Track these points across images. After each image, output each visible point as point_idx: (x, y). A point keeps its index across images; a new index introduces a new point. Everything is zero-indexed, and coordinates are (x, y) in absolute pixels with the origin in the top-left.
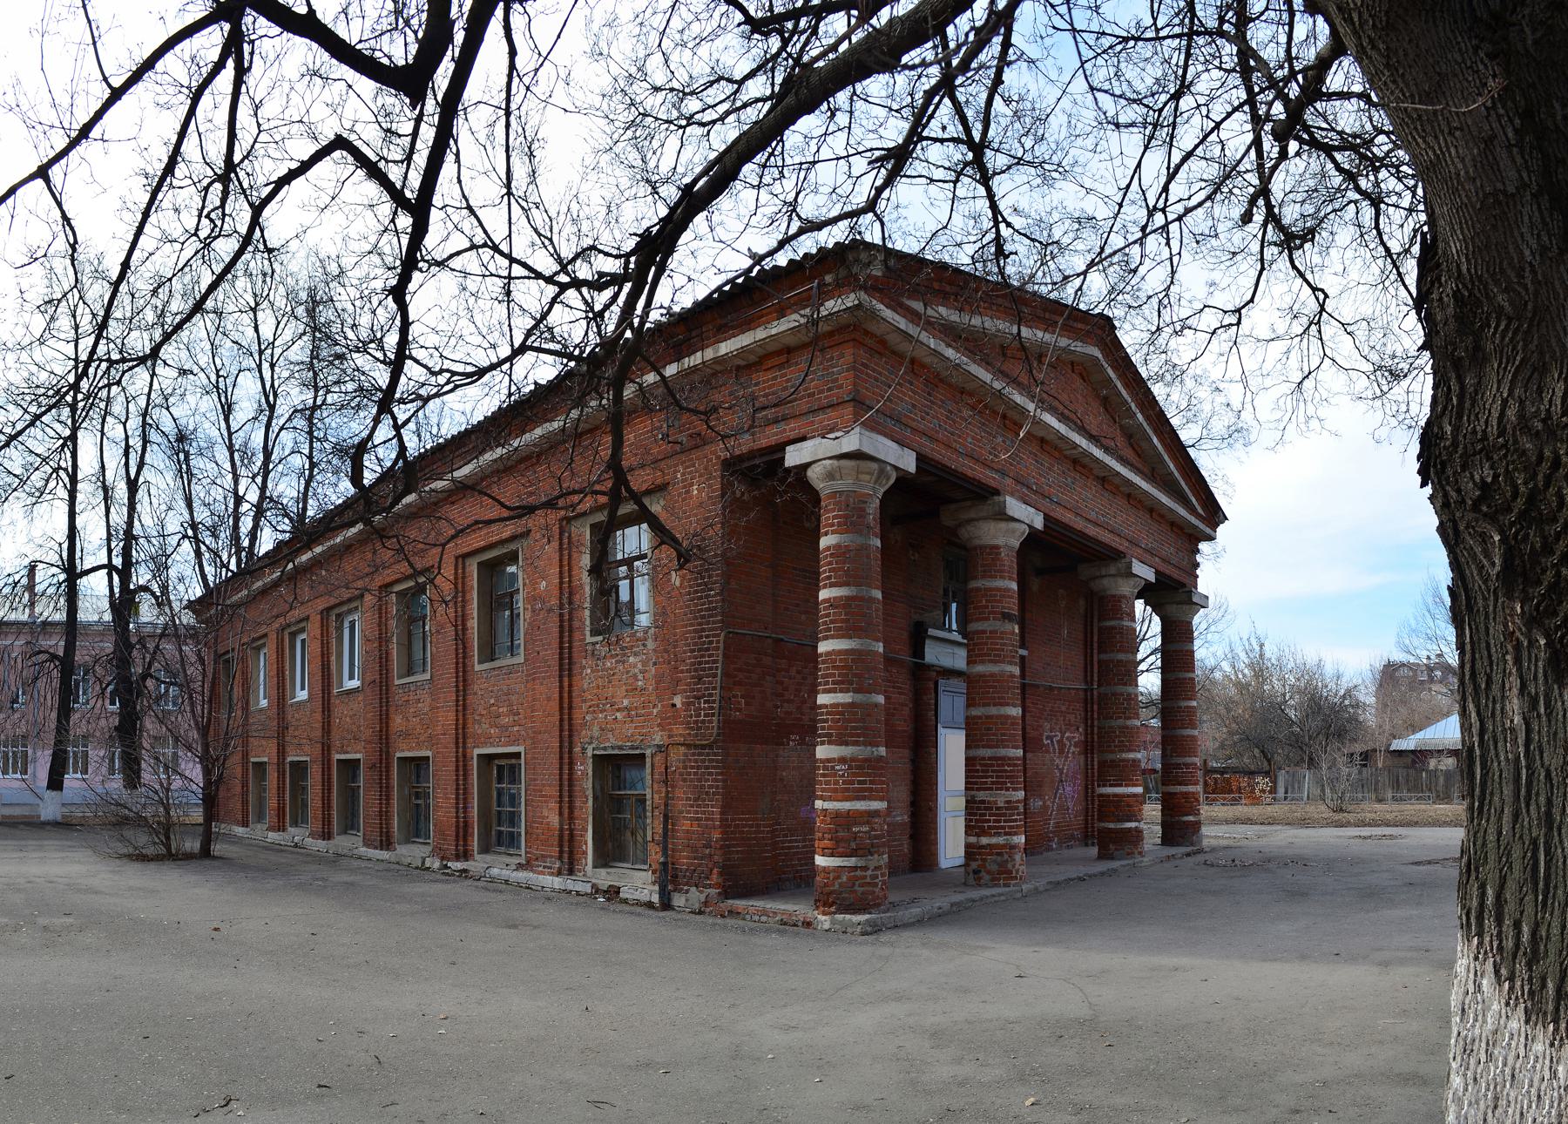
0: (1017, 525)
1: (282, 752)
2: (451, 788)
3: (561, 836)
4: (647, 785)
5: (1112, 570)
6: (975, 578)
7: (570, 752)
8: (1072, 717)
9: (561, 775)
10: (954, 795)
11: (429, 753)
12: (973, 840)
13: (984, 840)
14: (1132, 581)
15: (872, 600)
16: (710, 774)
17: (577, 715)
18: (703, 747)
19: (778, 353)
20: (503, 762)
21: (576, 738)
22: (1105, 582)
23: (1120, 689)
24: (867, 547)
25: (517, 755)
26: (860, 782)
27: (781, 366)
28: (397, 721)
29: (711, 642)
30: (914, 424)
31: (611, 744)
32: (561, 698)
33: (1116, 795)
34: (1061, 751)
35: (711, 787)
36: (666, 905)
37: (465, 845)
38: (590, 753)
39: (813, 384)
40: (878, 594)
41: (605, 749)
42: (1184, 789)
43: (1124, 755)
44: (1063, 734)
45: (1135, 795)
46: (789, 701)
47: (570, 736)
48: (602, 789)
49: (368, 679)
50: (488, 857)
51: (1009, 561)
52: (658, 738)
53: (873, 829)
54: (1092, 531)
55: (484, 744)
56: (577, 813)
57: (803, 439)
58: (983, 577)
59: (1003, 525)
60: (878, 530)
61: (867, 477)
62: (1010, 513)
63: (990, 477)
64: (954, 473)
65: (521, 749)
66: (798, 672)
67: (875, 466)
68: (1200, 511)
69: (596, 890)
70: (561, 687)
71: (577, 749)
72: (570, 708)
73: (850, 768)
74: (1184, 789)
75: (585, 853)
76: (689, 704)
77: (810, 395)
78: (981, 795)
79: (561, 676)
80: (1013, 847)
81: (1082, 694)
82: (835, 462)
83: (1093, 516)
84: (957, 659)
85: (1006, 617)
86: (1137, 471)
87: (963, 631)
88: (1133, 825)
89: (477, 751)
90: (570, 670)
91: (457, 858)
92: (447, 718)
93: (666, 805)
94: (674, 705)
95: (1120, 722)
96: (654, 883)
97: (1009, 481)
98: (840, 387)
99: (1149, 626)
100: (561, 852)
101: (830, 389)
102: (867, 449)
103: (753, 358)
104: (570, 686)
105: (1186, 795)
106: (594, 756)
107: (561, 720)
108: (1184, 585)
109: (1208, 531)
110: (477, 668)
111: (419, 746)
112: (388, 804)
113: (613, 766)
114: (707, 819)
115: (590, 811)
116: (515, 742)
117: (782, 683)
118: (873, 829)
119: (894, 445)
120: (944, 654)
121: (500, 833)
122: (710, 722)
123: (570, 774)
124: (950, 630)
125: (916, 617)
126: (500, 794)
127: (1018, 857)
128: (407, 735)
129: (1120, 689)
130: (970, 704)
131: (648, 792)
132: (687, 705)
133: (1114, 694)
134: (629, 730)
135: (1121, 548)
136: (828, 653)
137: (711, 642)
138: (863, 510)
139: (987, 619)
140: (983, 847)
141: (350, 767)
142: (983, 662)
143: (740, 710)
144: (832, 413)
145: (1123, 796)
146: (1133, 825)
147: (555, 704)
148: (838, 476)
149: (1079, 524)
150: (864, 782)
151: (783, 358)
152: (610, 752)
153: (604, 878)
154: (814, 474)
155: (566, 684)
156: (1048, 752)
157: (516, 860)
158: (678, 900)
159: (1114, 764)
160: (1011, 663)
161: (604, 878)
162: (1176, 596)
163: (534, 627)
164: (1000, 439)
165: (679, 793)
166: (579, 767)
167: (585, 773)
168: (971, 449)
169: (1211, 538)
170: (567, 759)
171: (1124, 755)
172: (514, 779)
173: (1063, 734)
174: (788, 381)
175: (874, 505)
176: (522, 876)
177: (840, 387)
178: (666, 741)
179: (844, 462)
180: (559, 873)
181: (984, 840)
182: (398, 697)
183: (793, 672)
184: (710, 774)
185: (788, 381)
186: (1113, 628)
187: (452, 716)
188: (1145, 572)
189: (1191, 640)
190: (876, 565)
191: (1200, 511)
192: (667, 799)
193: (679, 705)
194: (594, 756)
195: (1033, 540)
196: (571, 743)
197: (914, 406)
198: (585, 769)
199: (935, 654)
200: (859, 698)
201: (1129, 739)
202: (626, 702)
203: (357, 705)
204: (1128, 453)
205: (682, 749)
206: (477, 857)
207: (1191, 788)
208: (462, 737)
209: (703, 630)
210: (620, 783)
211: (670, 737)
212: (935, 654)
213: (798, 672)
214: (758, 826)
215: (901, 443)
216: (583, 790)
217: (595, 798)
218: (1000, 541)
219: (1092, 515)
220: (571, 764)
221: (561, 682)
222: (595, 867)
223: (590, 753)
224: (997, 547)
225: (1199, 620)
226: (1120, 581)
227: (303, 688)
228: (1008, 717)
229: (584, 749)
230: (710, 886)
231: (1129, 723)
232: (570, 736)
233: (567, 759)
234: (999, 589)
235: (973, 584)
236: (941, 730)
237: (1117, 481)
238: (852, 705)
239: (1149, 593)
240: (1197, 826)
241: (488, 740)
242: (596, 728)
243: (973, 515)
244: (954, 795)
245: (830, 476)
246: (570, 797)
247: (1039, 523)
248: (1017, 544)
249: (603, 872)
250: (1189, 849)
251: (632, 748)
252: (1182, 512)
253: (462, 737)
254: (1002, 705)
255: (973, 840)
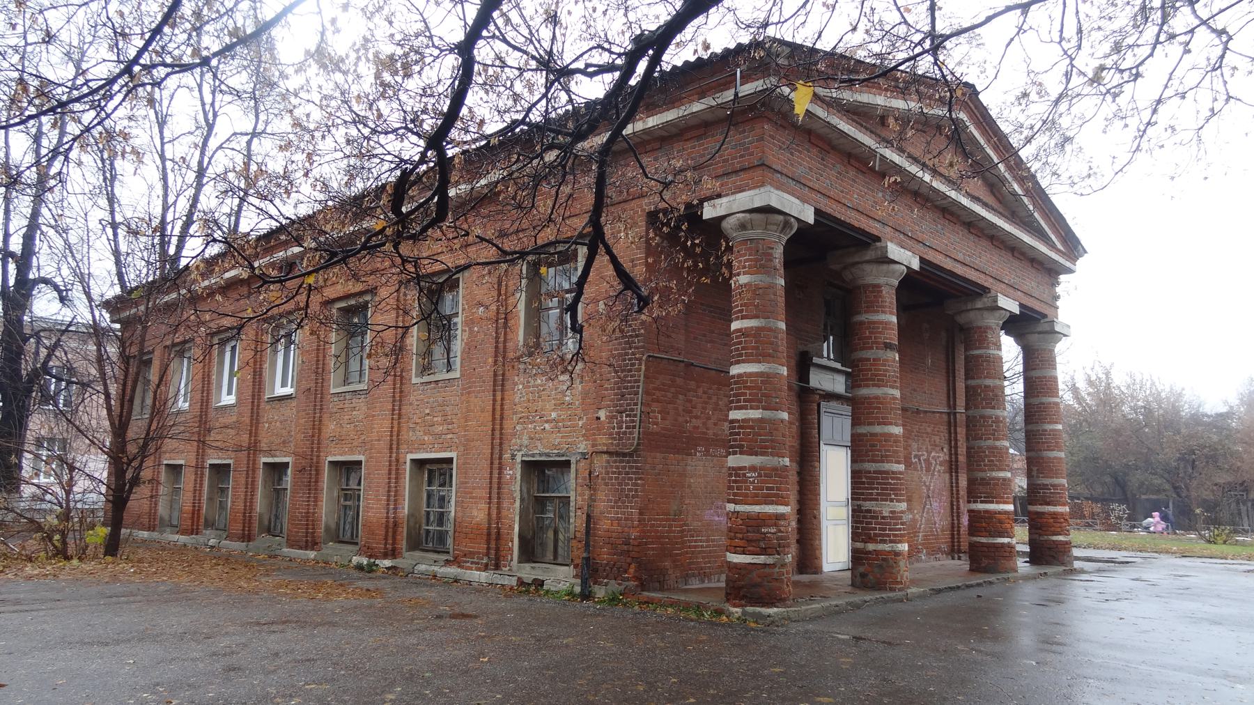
0: (897, 267)
1: (201, 455)
2: (383, 491)
3: (489, 534)
4: (572, 486)
5: (979, 305)
6: (859, 313)
7: (500, 458)
8: (937, 438)
9: (491, 478)
10: (836, 504)
11: (361, 458)
12: (859, 545)
13: (871, 547)
14: (997, 314)
15: (776, 331)
16: (630, 479)
17: (508, 425)
18: (624, 455)
19: (697, 127)
20: (434, 467)
21: (505, 446)
22: (972, 315)
23: (989, 412)
24: (771, 286)
25: (450, 461)
26: (768, 488)
27: (699, 137)
28: (330, 427)
29: (633, 365)
30: (810, 184)
31: (539, 451)
32: (494, 409)
33: (987, 511)
34: (928, 470)
35: (630, 490)
36: (586, 595)
37: (394, 543)
38: (519, 459)
39: (727, 152)
40: (782, 326)
41: (533, 455)
42: (1051, 509)
43: (995, 474)
44: (929, 453)
45: (1006, 513)
46: (697, 417)
47: (501, 444)
48: (528, 492)
49: (305, 385)
50: (417, 554)
51: (889, 297)
52: (583, 447)
53: (780, 531)
54: (959, 270)
55: (418, 450)
56: (504, 513)
57: (719, 196)
58: (867, 312)
59: (885, 267)
60: (782, 271)
61: (775, 227)
62: (891, 256)
63: (873, 228)
64: (843, 223)
65: (453, 455)
66: (704, 393)
67: (781, 218)
68: (1060, 246)
69: (521, 582)
70: (494, 400)
71: (507, 456)
72: (502, 418)
73: (760, 475)
74: (1051, 509)
75: (511, 549)
76: (612, 417)
77: (724, 161)
78: (867, 505)
79: (494, 391)
80: (897, 554)
81: (945, 417)
82: (747, 215)
83: (960, 257)
84: (838, 384)
85: (888, 346)
86: (1001, 215)
87: (840, 357)
88: (1006, 540)
89: (410, 456)
90: (503, 385)
91: (385, 556)
92: (382, 425)
93: (589, 506)
94: (598, 418)
95: (990, 442)
96: (575, 577)
97: (888, 229)
98: (752, 154)
99: (1009, 350)
100: (488, 548)
101: (742, 156)
102: (774, 204)
103: (674, 130)
104: (502, 399)
105: (1055, 516)
106: (523, 462)
107: (493, 430)
108: (1045, 316)
109: (1068, 264)
110: (414, 380)
111: (352, 452)
112: (316, 501)
113: (537, 470)
114: (626, 519)
115: (518, 511)
116: (449, 448)
117: (691, 401)
118: (780, 531)
119: (797, 201)
120: (828, 381)
121: (428, 532)
122: (631, 433)
123: (500, 478)
124: (822, 357)
125: (802, 348)
126: (429, 496)
127: (902, 564)
128: (340, 440)
129: (989, 412)
130: (855, 423)
131: (572, 495)
132: (611, 418)
133: (983, 417)
134: (556, 439)
135: (986, 284)
136: (740, 375)
137: (633, 365)
138: (771, 255)
139: (872, 348)
140: (870, 552)
141: (277, 469)
142: (868, 386)
143: (656, 424)
144: (742, 175)
145: (995, 513)
146: (1006, 540)
147: (488, 416)
148: (749, 226)
149: (948, 264)
150: (771, 489)
151: (702, 131)
152: (538, 458)
153: (528, 572)
154: (727, 225)
155: (499, 398)
156: (916, 469)
157: (444, 557)
158: (600, 592)
159: (985, 482)
160: (892, 387)
161: (528, 572)
162: (1032, 326)
163: (469, 348)
164: (880, 195)
165: (601, 495)
166: (508, 472)
167: (513, 477)
168: (860, 204)
169: (1070, 271)
170: (497, 464)
171: (995, 474)
172: (446, 481)
173: (929, 453)
174: (705, 149)
175: (779, 252)
176: (452, 571)
177: (752, 154)
178: (590, 450)
179: (755, 216)
180: (486, 568)
181: (871, 547)
182: (332, 405)
183: (700, 391)
184: (630, 479)
185: (705, 149)
186: (981, 356)
187: (387, 423)
188: (1010, 305)
189: (1054, 367)
190: (781, 301)
191: (1060, 246)
192: (592, 499)
193: (603, 418)
194: (523, 462)
195: (910, 282)
196: (501, 450)
197: (810, 169)
198: (514, 474)
199: (818, 380)
200: (768, 414)
201: (999, 458)
202: (554, 415)
203: (289, 411)
204: (990, 200)
205: (605, 457)
206: (406, 554)
207: (1059, 509)
208: (395, 443)
209: (627, 354)
210: (544, 483)
211: (593, 446)
212: (818, 380)
213: (704, 393)
214: (670, 526)
215: (804, 201)
216: (511, 493)
217: (522, 500)
218: (882, 281)
219: (960, 256)
220: (500, 469)
221: (494, 395)
222: (520, 562)
223: (519, 459)
224: (878, 286)
225: (1060, 348)
226: (986, 314)
227: (229, 393)
228: (891, 435)
229: (513, 457)
230: (628, 579)
231: (998, 443)
232: (501, 444)
233: (497, 464)
234: (881, 323)
235: (864, 317)
236: (823, 447)
237: (982, 224)
238: (761, 420)
239: (1014, 325)
240: (1067, 546)
241: (421, 446)
242: (525, 437)
243: (857, 259)
244: (836, 504)
245: (743, 226)
246: (499, 498)
247: (916, 265)
248: (896, 283)
249: (527, 566)
250: (1061, 568)
251: (558, 455)
252: (1043, 248)
253: (395, 443)
254: (885, 424)
255: (859, 545)
